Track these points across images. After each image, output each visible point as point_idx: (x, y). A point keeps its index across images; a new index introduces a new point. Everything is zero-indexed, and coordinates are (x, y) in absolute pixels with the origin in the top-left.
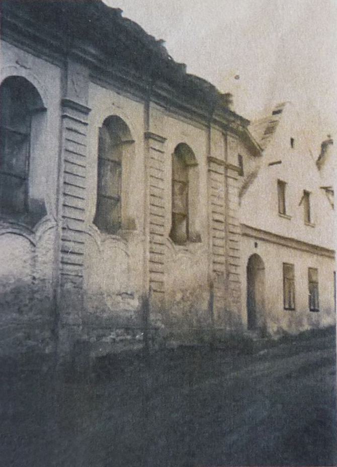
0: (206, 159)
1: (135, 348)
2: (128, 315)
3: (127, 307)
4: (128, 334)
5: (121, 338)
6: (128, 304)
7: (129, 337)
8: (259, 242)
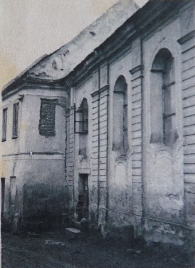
0: (5, 101)
1: (152, 237)
2: (173, 213)
3: (174, 207)
4: (173, 230)
5: (167, 231)
6: (175, 203)
7: (173, 232)
8: (106, 134)
